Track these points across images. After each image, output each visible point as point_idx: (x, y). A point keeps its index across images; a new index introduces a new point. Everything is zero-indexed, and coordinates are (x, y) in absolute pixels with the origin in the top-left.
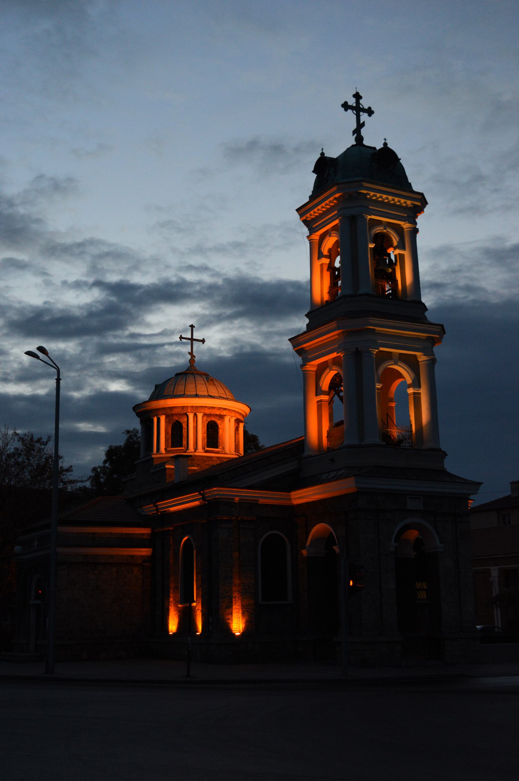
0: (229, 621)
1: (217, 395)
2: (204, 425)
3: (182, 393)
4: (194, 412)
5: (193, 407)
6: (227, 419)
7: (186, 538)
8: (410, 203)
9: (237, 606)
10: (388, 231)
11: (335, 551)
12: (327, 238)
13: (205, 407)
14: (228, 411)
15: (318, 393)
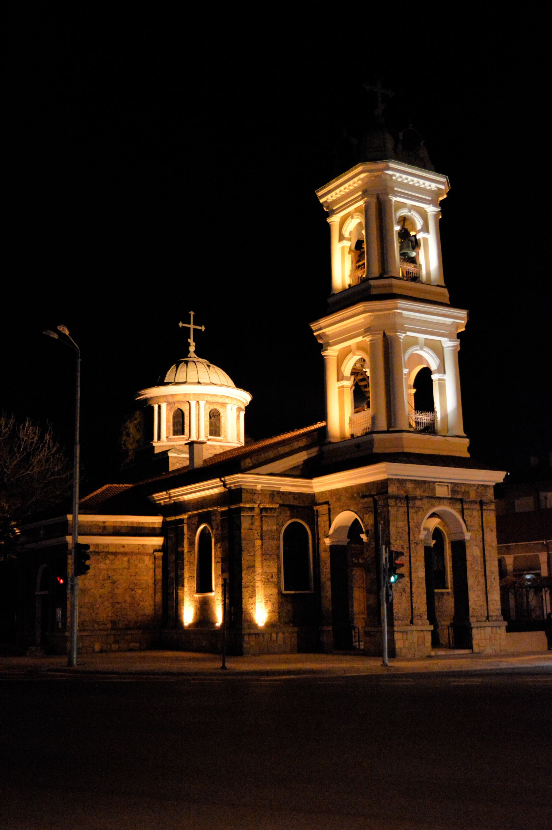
0: (251, 611)
2: (207, 413)
3: (185, 381)
4: (197, 399)
5: (195, 394)
6: (229, 407)
7: (202, 527)
9: (259, 595)
10: (412, 214)
11: (362, 539)
12: (349, 220)
13: (208, 394)
14: (230, 399)
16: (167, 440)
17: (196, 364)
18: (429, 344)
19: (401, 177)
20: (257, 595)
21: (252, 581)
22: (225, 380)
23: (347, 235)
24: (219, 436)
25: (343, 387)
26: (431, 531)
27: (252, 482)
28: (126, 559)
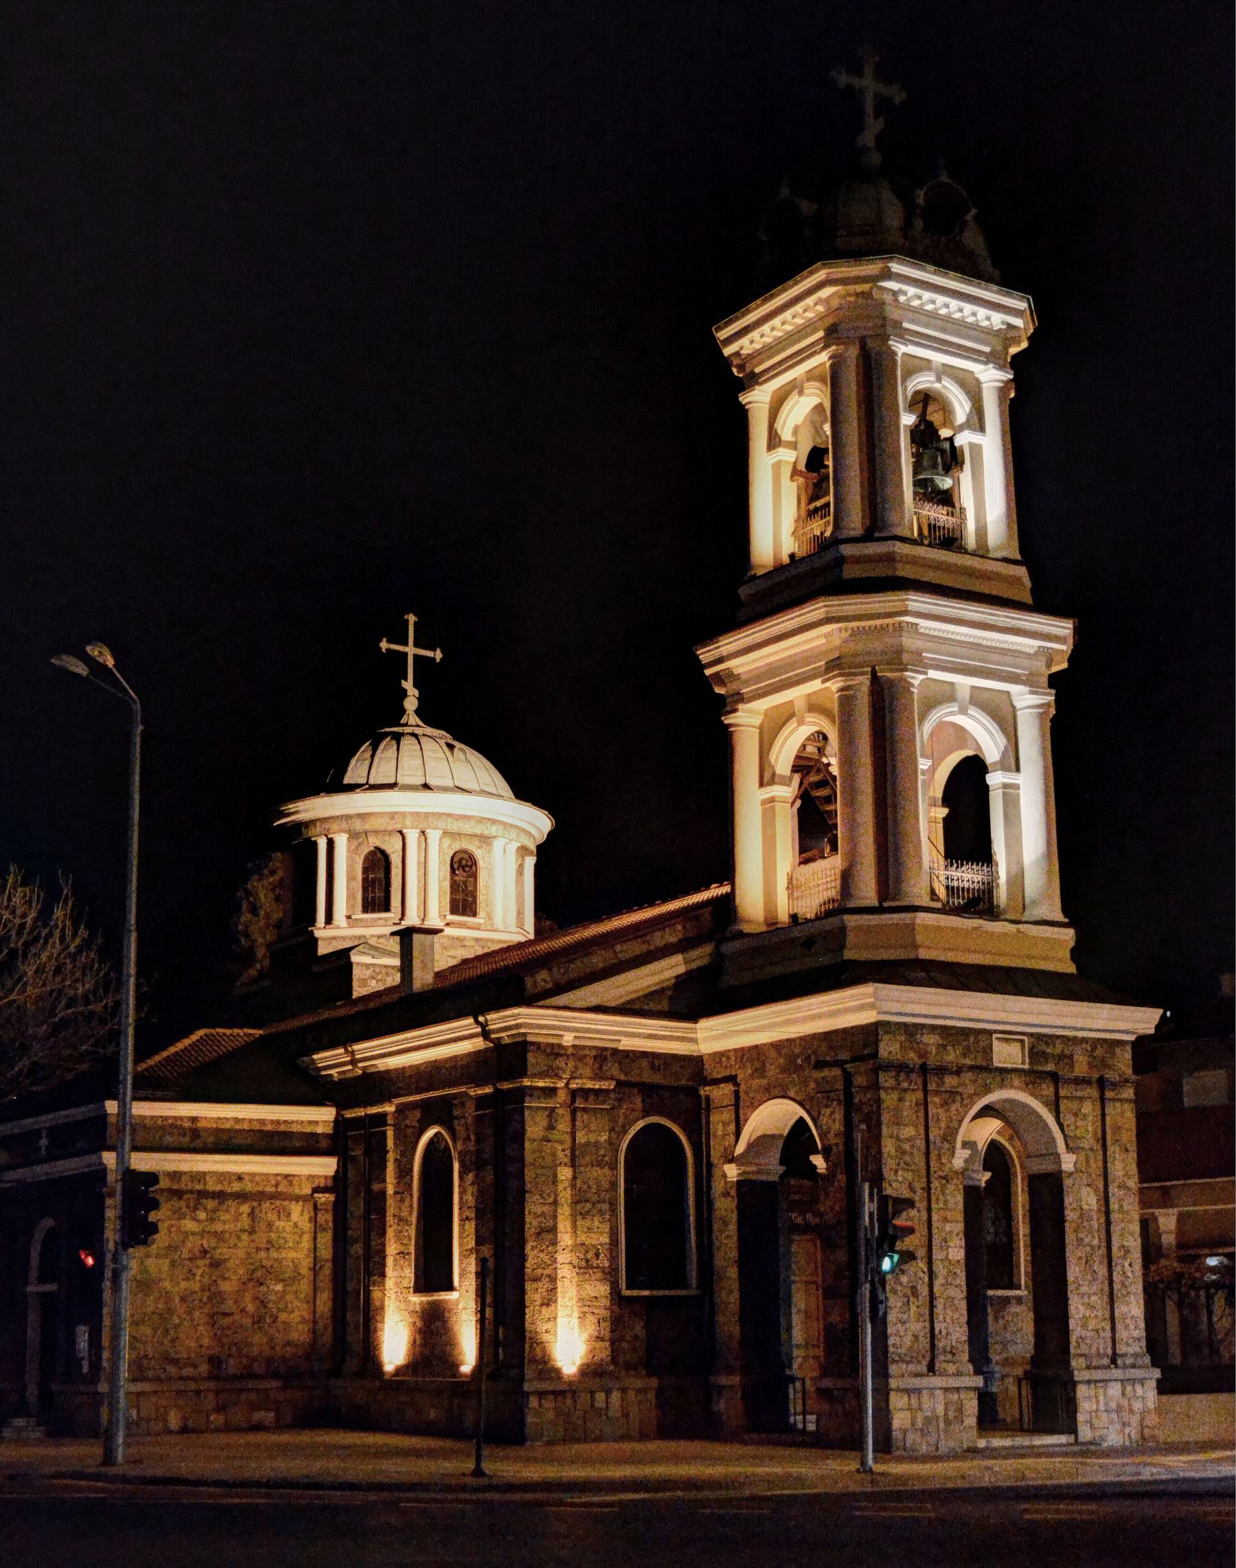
1: (476, 787)
3: (392, 781)
5: (418, 814)
6: (498, 845)
8: (1000, 321)
9: (567, 1299)
11: (815, 1167)
12: (794, 398)
13: (448, 815)
15: (766, 780)
16: (348, 924)
17: (419, 742)
18: (980, 700)
19: (919, 297)
20: (559, 1300)
24: (474, 914)
28: (245, 1208)
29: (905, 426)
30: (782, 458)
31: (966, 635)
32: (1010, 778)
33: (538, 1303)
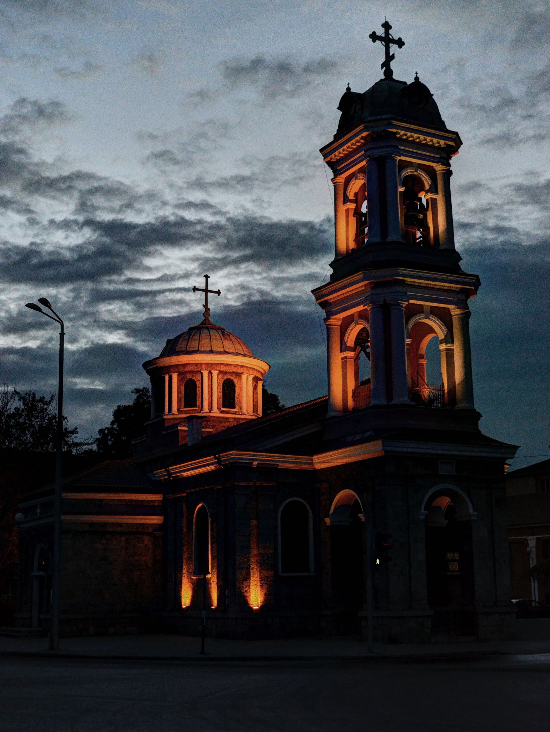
0: (247, 594)
3: (196, 349)
4: (209, 369)
5: (208, 363)
6: (244, 377)
7: (200, 505)
11: (361, 519)
12: (353, 181)
13: (221, 364)
14: (245, 369)
15: (343, 349)
16: (178, 412)
17: (209, 332)
18: (434, 312)
19: (406, 135)
20: (251, 578)
21: (246, 563)
22: (240, 348)
23: (351, 196)
24: (234, 407)
25: (347, 358)
26: (443, 509)
27: (249, 459)
28: (123, 538)
29: (400, 192)
30: (349, 207)
31: (426, 284)
32: (449, 346)
33: (242, 579)
